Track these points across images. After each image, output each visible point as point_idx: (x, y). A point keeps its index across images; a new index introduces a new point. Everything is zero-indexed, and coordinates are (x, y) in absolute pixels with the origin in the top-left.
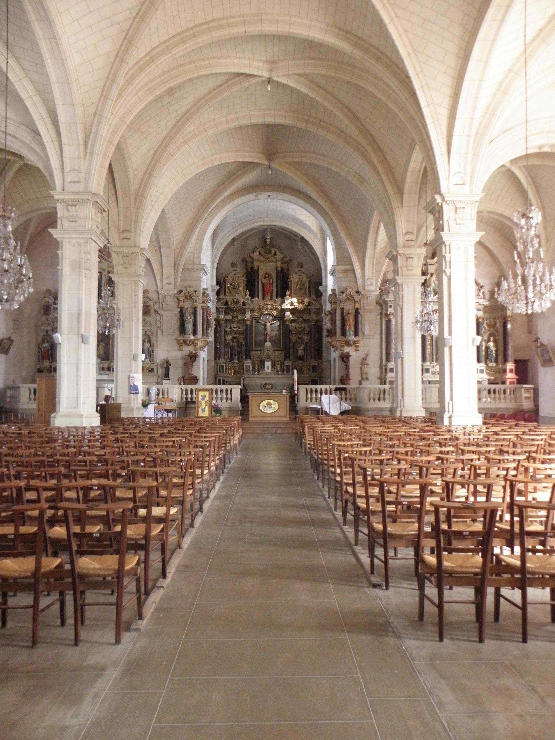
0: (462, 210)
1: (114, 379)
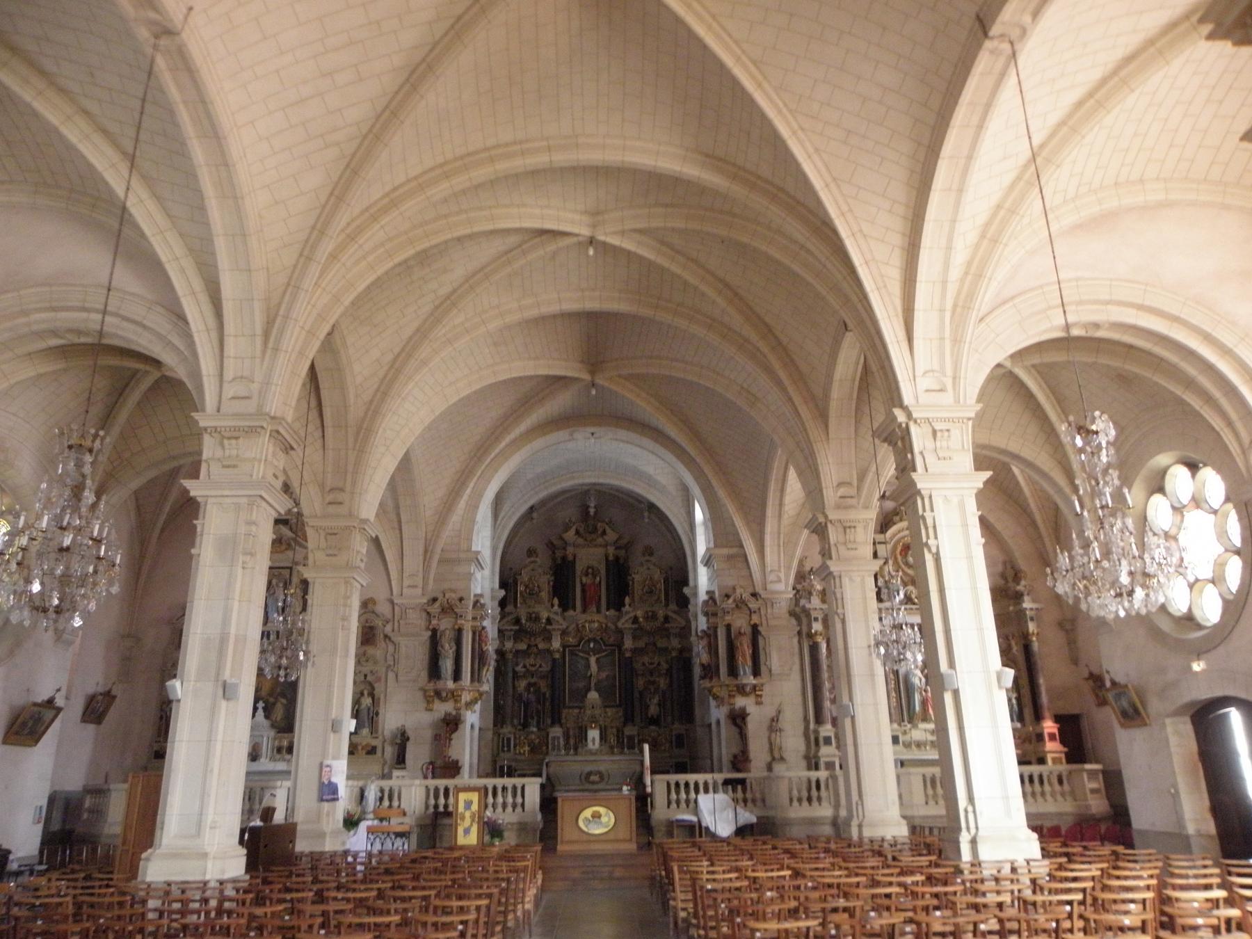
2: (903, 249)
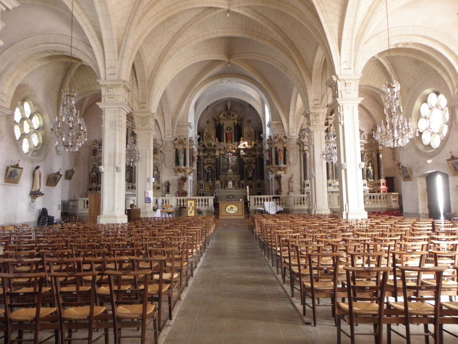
0: (350, 84)
1: (136, 194)
2: (340, 16)
